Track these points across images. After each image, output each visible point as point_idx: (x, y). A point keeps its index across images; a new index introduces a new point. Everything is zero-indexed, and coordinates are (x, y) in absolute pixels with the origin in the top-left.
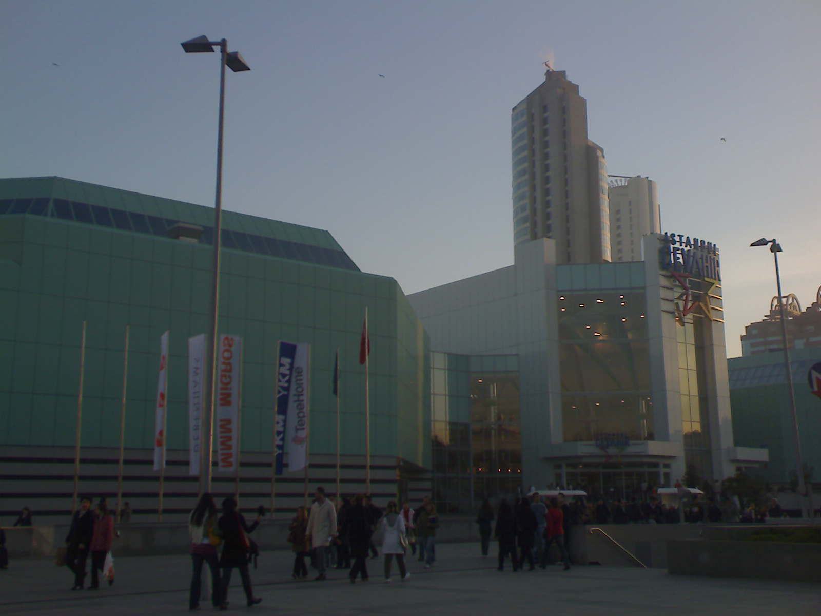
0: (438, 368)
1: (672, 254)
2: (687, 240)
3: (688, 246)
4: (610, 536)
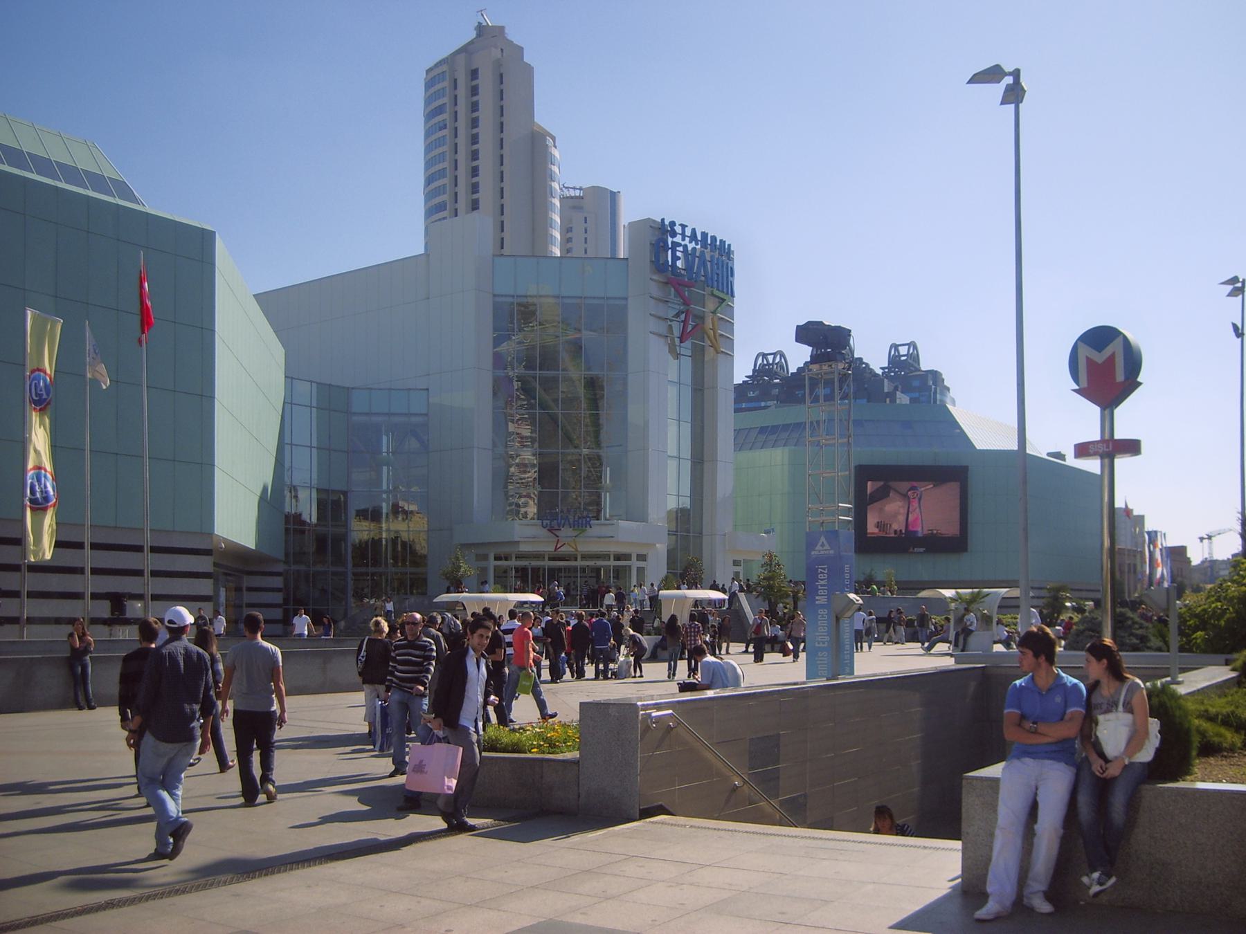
1: (670, 252)
2: (692, 233)
3: (694, 242)
4: (786, 796)
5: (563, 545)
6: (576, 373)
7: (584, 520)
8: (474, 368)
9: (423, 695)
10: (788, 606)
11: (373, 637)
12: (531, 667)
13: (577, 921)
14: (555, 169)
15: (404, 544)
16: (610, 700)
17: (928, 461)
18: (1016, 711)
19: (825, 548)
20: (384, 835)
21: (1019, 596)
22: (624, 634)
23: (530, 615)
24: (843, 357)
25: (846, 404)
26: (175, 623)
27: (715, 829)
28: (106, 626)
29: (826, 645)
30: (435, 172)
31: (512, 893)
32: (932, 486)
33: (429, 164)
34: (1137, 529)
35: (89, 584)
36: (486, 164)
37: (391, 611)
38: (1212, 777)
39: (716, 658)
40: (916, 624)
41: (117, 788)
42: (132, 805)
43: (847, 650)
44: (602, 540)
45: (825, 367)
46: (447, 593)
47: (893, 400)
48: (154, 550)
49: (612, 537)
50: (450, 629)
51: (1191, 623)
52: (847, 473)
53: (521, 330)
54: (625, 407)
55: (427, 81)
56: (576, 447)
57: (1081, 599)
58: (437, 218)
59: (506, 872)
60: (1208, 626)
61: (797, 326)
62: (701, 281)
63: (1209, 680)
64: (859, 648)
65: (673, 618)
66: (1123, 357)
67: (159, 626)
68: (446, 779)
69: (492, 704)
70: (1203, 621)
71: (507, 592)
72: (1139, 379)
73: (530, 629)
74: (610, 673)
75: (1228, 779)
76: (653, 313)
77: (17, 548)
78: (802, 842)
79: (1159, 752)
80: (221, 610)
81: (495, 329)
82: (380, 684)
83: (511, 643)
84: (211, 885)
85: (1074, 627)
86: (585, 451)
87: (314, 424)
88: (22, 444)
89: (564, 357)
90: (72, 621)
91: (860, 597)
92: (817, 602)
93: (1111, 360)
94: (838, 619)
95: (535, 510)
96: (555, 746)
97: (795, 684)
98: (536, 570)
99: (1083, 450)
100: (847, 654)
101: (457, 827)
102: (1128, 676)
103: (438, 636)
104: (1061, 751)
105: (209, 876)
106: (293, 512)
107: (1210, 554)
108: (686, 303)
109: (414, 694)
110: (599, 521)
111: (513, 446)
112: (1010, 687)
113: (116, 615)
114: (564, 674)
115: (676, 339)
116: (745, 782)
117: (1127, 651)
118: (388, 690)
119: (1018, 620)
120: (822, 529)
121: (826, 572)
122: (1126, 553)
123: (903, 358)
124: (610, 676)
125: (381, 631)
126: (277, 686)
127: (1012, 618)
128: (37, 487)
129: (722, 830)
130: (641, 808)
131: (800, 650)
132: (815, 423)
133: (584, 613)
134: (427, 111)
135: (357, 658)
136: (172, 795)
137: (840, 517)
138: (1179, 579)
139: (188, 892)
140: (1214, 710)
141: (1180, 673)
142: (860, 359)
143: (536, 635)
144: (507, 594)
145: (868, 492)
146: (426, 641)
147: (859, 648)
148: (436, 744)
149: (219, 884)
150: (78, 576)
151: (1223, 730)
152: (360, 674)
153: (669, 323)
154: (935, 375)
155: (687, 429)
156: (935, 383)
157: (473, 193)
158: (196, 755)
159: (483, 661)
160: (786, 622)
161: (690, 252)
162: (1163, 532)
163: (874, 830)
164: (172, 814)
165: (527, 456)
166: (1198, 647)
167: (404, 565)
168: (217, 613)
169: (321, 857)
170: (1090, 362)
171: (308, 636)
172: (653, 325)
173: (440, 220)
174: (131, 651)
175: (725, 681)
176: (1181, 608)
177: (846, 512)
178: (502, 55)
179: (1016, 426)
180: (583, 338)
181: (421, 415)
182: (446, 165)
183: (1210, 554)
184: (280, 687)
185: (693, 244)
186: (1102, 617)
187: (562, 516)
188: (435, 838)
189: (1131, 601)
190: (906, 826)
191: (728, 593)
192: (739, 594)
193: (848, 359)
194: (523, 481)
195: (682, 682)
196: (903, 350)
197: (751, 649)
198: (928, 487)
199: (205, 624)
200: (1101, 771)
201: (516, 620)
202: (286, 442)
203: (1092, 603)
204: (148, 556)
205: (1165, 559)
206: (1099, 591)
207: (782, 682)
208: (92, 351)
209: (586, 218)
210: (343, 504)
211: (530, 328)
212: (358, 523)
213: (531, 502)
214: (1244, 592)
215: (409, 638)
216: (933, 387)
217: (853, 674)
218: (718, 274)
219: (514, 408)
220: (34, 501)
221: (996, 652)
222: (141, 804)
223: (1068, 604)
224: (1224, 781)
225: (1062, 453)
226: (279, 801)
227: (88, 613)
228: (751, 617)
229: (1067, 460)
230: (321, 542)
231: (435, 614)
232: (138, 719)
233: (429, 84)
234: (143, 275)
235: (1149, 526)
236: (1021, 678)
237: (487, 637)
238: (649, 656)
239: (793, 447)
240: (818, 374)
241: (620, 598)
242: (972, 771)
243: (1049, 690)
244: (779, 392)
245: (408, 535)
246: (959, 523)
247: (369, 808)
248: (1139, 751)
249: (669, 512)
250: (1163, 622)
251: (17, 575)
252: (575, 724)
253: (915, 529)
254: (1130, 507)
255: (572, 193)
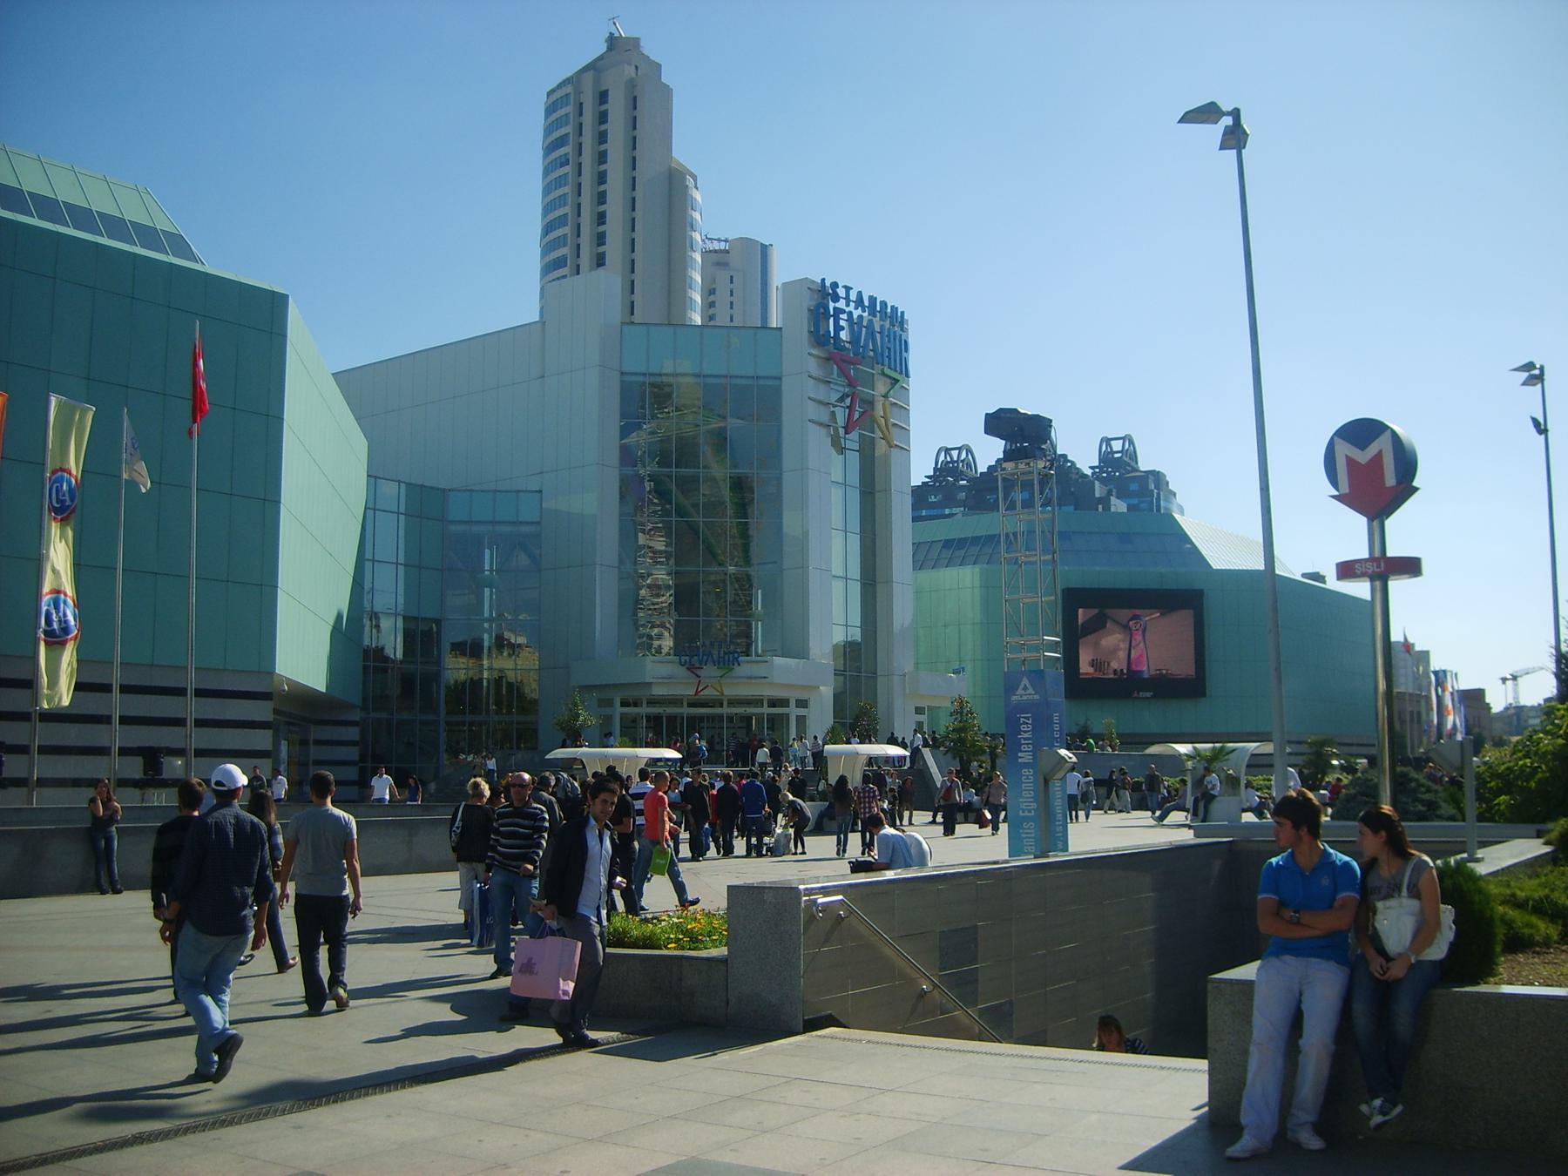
0: (375, 503)
1: (832, 320)
3: (860, 308)
5: (705, 688)
6: (720, 471)
7: (731, 656)
8: (598, 464)
9: (532, 876)
10: (984, 765)
11: (470, 803)
12: (667, 840)
13: (727, 1160)
14: (696, 215)
15: (510, 685)
16: (764, 882)
17: (1153, 584)
18: (1274, 897)
19: (1028, 692)
20: (483, 1051)
21: (1272, 752)
22: (781, 800)
23: (665, 775)
24: (1044, 454)
26: (224, 786)
27: (898, 1045)
28: (137, 789)
29: (1033, 813)
30: (555, 219)
31: (644, 1124)
32: (1158, 614)
33: (547, 209)
34: (1421, 668)
35: (116, 736)
36: (615, 209)
37: (493, 770)
38: (1521, 979)
39: (897, 829)
40: (1144, 788)
41: (146, 992)
42: (166, 1013)
43: (1059, 821)
44: (753, 681)
45: (1022, 466)
46: (562, 747)
47: (1107, 507)
48: (200, 693)
49: (765, 677)
50: (566, 793)
51: (1493, 784)
52: (1053, 598)
53: (654, 417)
54: (780, 515)
55: (548, 105)
56: (720, 565)
57: (1352, 755)
58: (554, 277)
59: (637, 1098)
60: (1514, 789)
61: (987, 414)
62: (869, 357)
63: (1516, 857)
64: (1074, 817)
65: (842, 780)
66: (1392, 456)
67: (203, 789)
68: (561, 981)
69: (619, 887)
70: (1507, 781)
71: (636, 747)
72: (1415, 484)
73: (665, 793)
74: (765, 848)
75: (1542, 981)
76: (812, 396)
77: (27, 692)
78: (1007, 1061)
79: (1453, 947)
80: (282, 769)
81: (623, 416)
82: (479, 862)
83: (642, 810)
84: (266, 1115)
85: (1344, 791)
86: (732, 569)
87: (402, 533)
88: (36, 563)
89: (706, 452)
90: (94, 783)
91: (1073, 753)
92: (1020, 760)
93: (1378, 459)
94: (1046, 781)
95: (672, 644)
96: (697, 941)
97: (995, 863)
98: (672, 719)
99: (1347, 570)
100: (1059, 825)
101: (574, 1042)
102: (1413, 852)
103: (551, 802)
104: (1329, 947)
105: (262, 1103)
106: (374, 646)
107: (1516, 698)
108: (851, 384)
109: (521, 874)
110: (749, 658)
111: (644, 562)
112: (1264, 867)
113: (150, 775)
114: (708, 849)
115: (840, 429)
116: (935, 986)
117: (1411, 821)
118: (488, 871)
119: (1272, 783)
120: (1023, 669)
121: (1030, 722)
122: (1407, 698)
123: (1117, 455)
124: (764, 852)
125: (482, 795)
126: (351, 865)
127: (1264, 780)
128: (54, 615)
129: (907, 1046)
130: (806, 1018)
131: (1001, 820)
132: (1011, 535)
133: (731, 773)
134: (547, 143)
135: (451, 828)
136: (218, 1001)
137: (1046, 654)
138: (1476, 730)
139: (236, 1124)
140: (1524, 894)
141: (1480, 848)
142: (1064, 456)
143: (673, 800)
144: (636, 749)
145: (1080, 622)
146: (536, 808)
147: (1074, 817)
148: (548, 937)
149: (275, 1114)
150: (103, 727)
151: (1534, 919)
152: (454, 849)
153: (832, 409)
154: (1157, 476)
155: (855, 542)
156: (1157, 487)
157: (599, 245)
158: (247, 952)
159: (607, 834)
160: (982, 784)
161: (855, 321)
162: (1454, 672)
163: (1098, 1046)
164: (216, 1025)
165: (661, 575)
166: (1502, 814)
167: (509, 712)
168: (276, 772)
169: (405, 1080)
170: (1351, 462)
171: (389, 802)
173: (558, 279)
174: (168, 820)
175: (908, 860)
176: (1479, 767)
177: (1053, 647)
178: (637, 75)
179: (1261, 540)
180: (728, 428)
181: (533, 523)
182: (566, 210)
183: (1516, 698)
184: (354, 866)
185: (859, 311)
186: (1378, 777)
187: (703, 651)
188: (547, 1056)
189: (1415, 758)
190: (1138, 1041)
191: (909, 749)
192: (923, 750)
193: (1049, 455)
194: (656, 607)
195: (854, 860)
196: (1117, 446)
197: (939, 819)
198: (1153, 616)
199: (262, 786)
200: (1382, 972)
201: (648, 782)
202: (367, 557)
203: (1365, 761)
204: (191, 700)
205: (1458, 705)
206: (1374, 745)
207: (978, 861)
208: (130, 444)
209: (732, 277)
210: (435, 635)
211: (664, 415)
212: (454, 659)
213: (666, 634)
214: (1560, 745)
215: (516, 804)
216: (1156, 491)
217: (1067, 850)
218: (889, 349)
219: (645, 515)
220: (49, 633)
221: (1246, 822)
222: (178, 1012)
223: (1335, 762)
224: (1536, 983)
225: (1321, 573)
226: (351, 1008)
227: (115, 775)
228: (938, 779)
229: (1327, 583)
230: (408, 683)
231: (547, 774)
232: (175, 906)
233: (550, 110)
234: (197, 351)
235: (1436, 664)
236: (1278, 855)
237: (613, 803)
238: (812, 828)
239: (985, 566)
240: (1013, 474)
241: (777, 755)
242: (1219, 972)
243: (1314, 870)
244: (966, 497)
245: (516, 673)
246: (1194, 661)
247: (464, 1017)
248: (1429, 946)
249: (835, 647)
250: (1456, 784)
251: (25, 726)
252: (722, 913)
253: (1138, 669)
254: (1410, 640)
255: (716, 245)
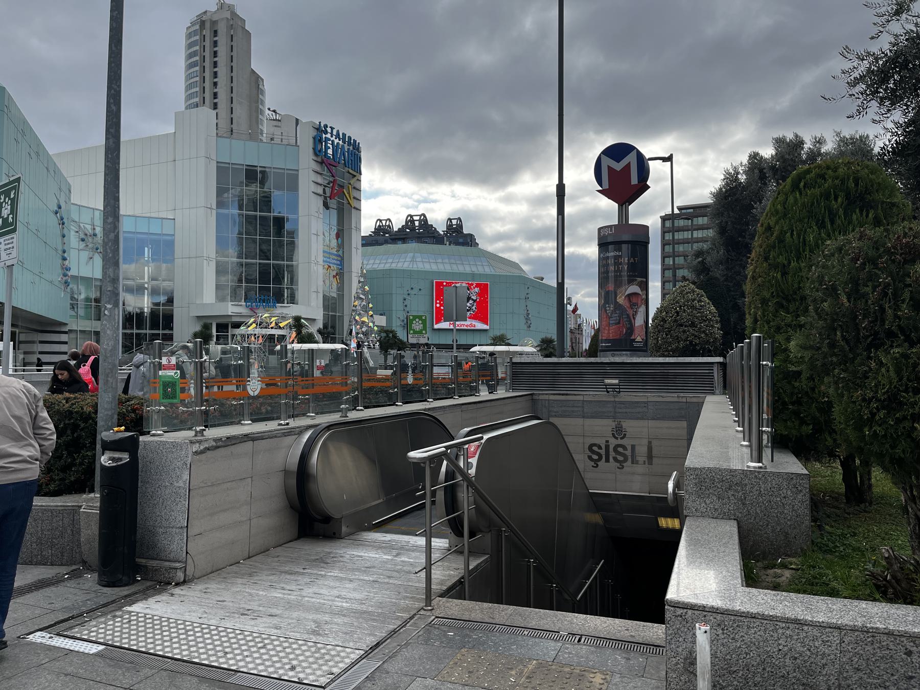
25: (416, 548)
93: (628, 166)
154: (471, 236)
156: (471, 241)
172: (313, 188)
196: (454, 222)
